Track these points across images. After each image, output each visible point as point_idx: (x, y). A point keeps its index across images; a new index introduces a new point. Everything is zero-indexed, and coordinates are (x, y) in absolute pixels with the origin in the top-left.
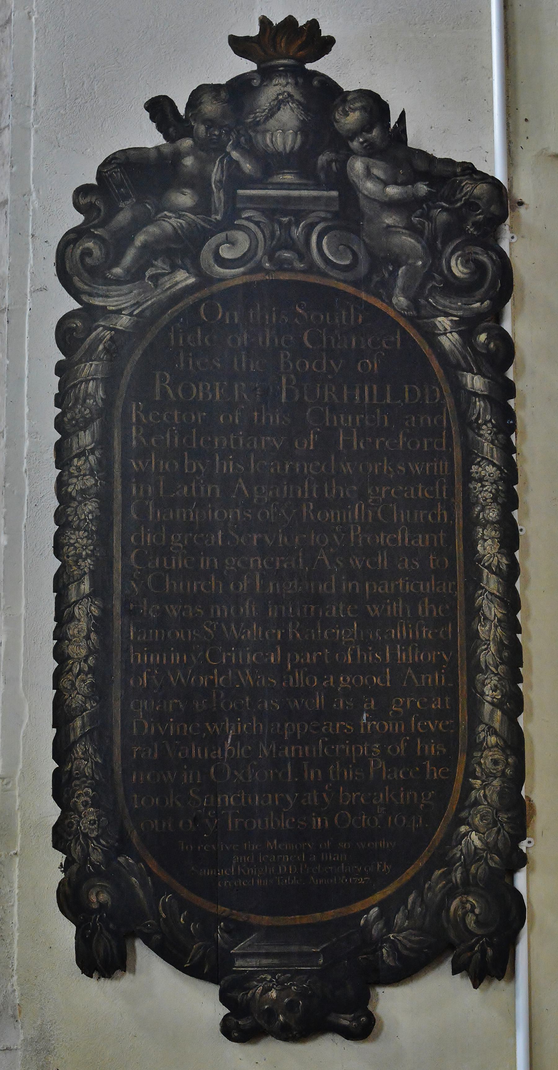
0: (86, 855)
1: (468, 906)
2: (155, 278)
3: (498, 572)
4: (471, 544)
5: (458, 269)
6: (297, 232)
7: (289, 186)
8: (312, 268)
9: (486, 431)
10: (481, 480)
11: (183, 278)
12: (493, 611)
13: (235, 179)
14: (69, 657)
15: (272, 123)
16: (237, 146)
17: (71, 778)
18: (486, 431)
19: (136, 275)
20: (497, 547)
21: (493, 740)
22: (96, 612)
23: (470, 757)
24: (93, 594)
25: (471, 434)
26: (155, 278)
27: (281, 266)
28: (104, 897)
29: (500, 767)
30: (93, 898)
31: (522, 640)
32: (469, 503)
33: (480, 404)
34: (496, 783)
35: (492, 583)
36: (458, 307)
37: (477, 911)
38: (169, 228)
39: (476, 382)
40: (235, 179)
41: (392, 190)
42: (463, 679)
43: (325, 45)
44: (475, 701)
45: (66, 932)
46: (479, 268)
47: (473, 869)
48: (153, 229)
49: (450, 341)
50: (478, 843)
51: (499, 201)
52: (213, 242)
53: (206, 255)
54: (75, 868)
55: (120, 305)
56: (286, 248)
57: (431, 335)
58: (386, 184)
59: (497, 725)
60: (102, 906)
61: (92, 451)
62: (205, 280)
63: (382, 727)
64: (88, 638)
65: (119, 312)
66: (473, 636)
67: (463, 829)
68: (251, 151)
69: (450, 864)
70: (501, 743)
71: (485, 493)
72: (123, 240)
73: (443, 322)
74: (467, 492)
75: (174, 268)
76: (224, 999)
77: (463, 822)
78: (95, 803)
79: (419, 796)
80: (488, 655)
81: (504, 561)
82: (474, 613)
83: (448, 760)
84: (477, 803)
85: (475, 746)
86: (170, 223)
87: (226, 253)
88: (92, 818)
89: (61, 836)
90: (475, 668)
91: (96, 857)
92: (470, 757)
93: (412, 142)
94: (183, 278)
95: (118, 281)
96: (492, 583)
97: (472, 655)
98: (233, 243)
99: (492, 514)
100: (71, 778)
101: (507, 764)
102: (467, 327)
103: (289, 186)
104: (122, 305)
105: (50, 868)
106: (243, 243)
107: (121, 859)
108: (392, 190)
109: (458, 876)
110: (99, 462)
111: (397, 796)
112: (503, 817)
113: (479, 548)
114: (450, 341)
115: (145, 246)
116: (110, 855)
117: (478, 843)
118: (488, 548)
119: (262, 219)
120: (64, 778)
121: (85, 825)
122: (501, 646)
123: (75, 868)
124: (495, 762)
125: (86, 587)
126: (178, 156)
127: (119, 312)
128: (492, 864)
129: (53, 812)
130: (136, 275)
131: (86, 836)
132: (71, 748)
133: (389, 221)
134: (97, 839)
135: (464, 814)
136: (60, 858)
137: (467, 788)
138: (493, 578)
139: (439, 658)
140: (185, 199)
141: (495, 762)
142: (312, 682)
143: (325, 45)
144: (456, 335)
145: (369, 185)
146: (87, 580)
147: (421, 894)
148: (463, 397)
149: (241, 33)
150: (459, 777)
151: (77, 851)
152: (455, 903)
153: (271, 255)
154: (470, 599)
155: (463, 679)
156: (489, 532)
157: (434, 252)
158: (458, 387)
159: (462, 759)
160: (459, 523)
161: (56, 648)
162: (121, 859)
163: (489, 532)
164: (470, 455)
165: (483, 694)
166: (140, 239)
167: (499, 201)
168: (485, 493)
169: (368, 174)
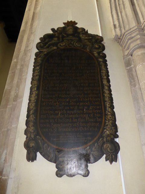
0: (31, 136)
1: (108, 146)
2: (51, 48)
3: (107, 86)
4: (102, 82)
5: (97, 46)
6: (72, 43)
7: (71, 37)
8: (75, 46)
9: (103, 66)
10: (103, 73)
11: (55, 48)
12: (107, 92)
13: (63, 37)
14: (31, 100)
15: (69, 31)
16: (64, 33)
17: (29, 121)
18: (103, 66)
19: (48, 47)
20: (106, 82)
21: (109, 113)
22: (37, 93)
23: (105, 117)
24: (37, 90)
25: (100, 66)
26: (51, 48)
27: (70, 46)
28: (33, 145)
29: (111, 118)
30: (31, 145)
31: (27, 11)
32: (101, 76)
33: (102, 63)
34: (111, 121)
35: (106, 88)
36: (97, 51)
37: (110, 147)
38: (53, 42)
39: (101, 60)
40: (63, 37)
41: (86, 38)
42: (103, 103)
43: (77, 23)
44: (105, 107)
45: (25, 151)
46: (100, 46)
47: (108, 139)
48: (51, 42)
49: (96, 55)
50: (108, 133)
51: (101, 39)
52: (60, 43)
53: (59, 45)
54: (28, 138)
55: (139, 6)
56: (71, 44)
57: (93, 54)
58: (85, 37)
59: (110, 111)
60: (33, 146)
61: (39, 69)
62: (58, 48)
63: (88, 112)
64: (35, 97)
65: (45, 52)
66: (104, 96)
67: (105, 130)
68: (66, 34)
69: (103, 137)
70: (111, 114)
71: (104, 74)
72: (47, 43)
73: (95, 53)
74: (101, 75)
75: (54, 47)
76: (57, 167)
77: (105, 129)
78: (33, 126)
79: (96, 124)
80: (107, 99)
81: (108, 84)
82: (103, 92)
83: (101, 117)
84: (107, 125)
85: (106, 115)
86: (53, 42)
87: (61, 45)
88: (32, 129)
89: (26, 132)
90: (105, 101)
91: (33, 136)
92: (105, 117)
93: (89, 33)
94: (55, 48)
95: (45, 48)
96: (106, 88)
97: (104, 99)
98: (63, 44)
99: (105, 77)
100: (29, 121)
101: (113, 118)
102: (99, 53)
103: (71, 37)
104: (45, 51)
105: (24, 138)
106: (64, 44)
107: (37, 137)
108: (86, 38)
109: (105, 140)
110: (40, 71)
111: (92, 124)
112: (113, 128)
113: (103, 82)
114: (96, 55)
115: (50, 44)
116: (35, 136)
117: (108, 133)
118: (105, 82)
119: (67, 41)
120: (28, 121)
121: (31, 130)
122: (109, 97)
123: (28, 138)
124: (110, 118)
125: (35, 89)
126: (55, 34)
127: (45, 52)
128: (112, 137)
129: (25, 127)
130: (48, 47)
131: (31, 132)
132: (30, 116)
133: (86, 41)
134: (33, 133)
135: (105, 127)
136: (25, 136)
137: (105, 123)
138: (106, 87)
139: (98, 100)
140: (56, 39)
141: (110, 118)
142: (75, 104)
143: (77, 23)
144: (97, 54)
145: (83, 37)
146: (36, 88)
147: (98, 144)
148: (99, 62)
149: (65, 22)
150: (103, 120)
151: (29, 135)
152: (105, 145)
153: (68, 45)
154: (103, 90)
155: (103, 103)
156: (105, 80)
157: (93, 44)
158: (98, 61)
159: (104, 117)
160: (100, 79)
161: (29, 99)
162: (37, 137)
163: (105, 80)
164: (101, 70)
165: (106, 106)
166: (49, 43)
167: (101, 39)
168: (104, 74)
169: (83, 36)
